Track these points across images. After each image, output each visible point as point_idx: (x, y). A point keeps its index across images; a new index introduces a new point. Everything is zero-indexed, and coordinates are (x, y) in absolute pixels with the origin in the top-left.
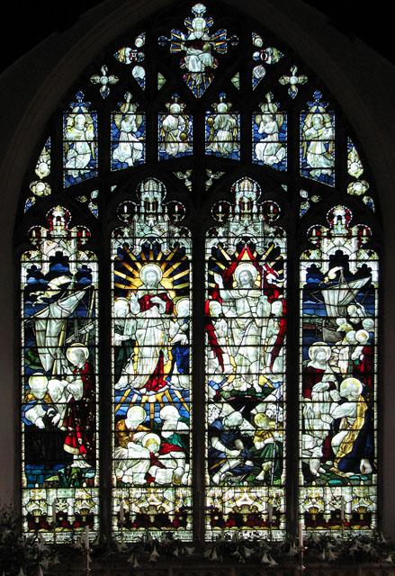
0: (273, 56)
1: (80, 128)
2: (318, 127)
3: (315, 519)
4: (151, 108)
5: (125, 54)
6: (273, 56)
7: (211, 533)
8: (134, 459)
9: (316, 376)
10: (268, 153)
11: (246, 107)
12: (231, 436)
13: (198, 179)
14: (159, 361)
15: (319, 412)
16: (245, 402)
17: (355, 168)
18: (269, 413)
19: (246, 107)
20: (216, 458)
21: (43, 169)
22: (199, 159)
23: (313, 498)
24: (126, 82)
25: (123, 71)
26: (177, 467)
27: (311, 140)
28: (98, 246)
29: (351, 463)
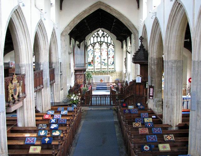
0: (106, 34)
1: (92, 39)
2: (109, 38)
3: (110, 69)
4: (97, 37)
5: (95, 34)
6: (106, 34)
7: (102, 70)
8: (96, 64)
9: (109, 58)
10: (106, 41)
11: (104, 37)
12: (103, 62)
13: (101, 43)
14: (123, 134)
15: (109, 60)
16: (104, 60)
17: (112, 42)
18: (106, 61)
19: (104, 37)
20: (102, 64)
21: (89, 42)
22: (101, 42)
23: (109, 67)
24: (95, 36)
25: (95, 35)
26: (100, 65)
27: (197, 114)
28: (93, 48)
29: (112, 64)
